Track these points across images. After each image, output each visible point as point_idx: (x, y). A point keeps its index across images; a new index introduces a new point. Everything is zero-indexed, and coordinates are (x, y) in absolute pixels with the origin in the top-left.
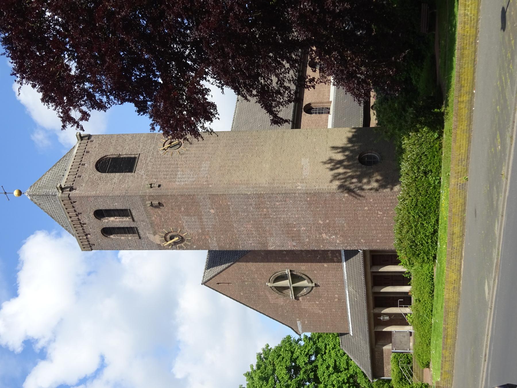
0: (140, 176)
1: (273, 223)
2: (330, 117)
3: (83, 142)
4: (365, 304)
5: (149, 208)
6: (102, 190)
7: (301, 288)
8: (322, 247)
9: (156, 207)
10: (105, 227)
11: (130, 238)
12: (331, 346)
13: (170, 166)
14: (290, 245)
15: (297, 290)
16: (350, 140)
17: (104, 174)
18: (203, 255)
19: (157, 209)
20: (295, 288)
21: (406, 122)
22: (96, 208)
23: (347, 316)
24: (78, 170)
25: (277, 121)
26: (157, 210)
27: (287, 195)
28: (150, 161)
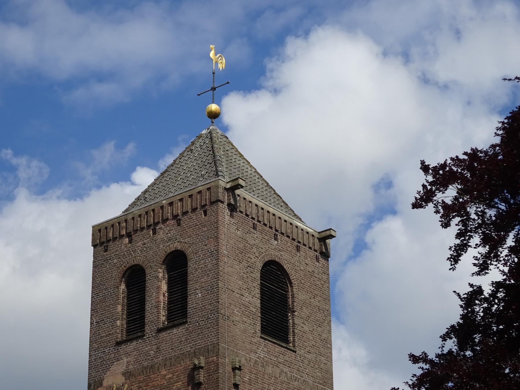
0: (254, 348)
3: (316, 241)
5: (188, 363)
6: (230, 269)
10: (147, 271)
11: (118, 323)
17: (258, 275)
19: (186, 380)
24: (265, 225)
26: (184, 379)
28: (282, 371)
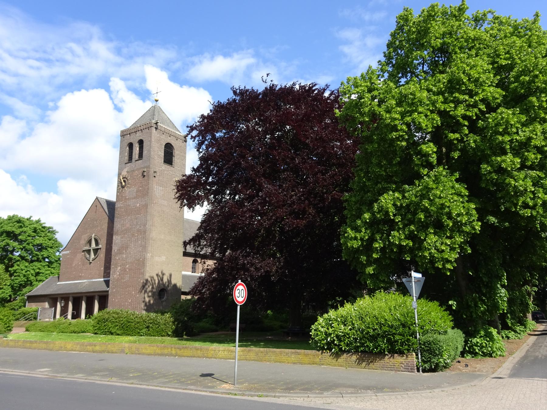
1: (129, 239)
2: (190, 273)
4: (76, 291)
7: (89, 254)
8: (112, 266)
9: (143, 174)
12: (53, 271)
13: (164, 184)
14: (115, 248)
15: (89, 251)
16: (175, 285)
18: (113, 199)
20: (90, 250)
21: (179, 316)
22: (144, 141)
23: (70, 281)
25: (185, 244)
27: (144, 248)
